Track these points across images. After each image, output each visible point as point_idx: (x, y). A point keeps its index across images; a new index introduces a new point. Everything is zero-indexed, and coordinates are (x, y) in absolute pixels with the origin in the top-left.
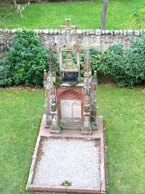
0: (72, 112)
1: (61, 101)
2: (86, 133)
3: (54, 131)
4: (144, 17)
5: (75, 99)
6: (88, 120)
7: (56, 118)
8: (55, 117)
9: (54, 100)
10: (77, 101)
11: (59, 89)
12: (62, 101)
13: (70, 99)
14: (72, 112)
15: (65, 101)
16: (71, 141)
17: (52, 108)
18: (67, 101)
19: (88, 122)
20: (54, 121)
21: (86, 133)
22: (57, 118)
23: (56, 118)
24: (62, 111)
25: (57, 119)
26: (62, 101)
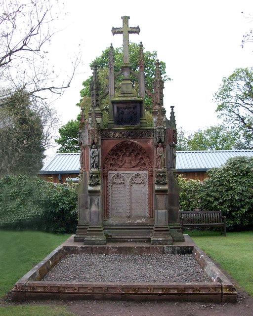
0: (131, 203)
1: (109, 172)
2: (161, 239)
3: (93, 239)
4: (125, 315)
5: (136, 168)
6: (164, 208)
7: (98, 203)
8: (96, 203)
9: (97, 159)
10: (140, 172)
11: (106, 142)
12: (112, 174)
13: (129, 168)
14: (131, 203)
15: (116, 173)
16: (133, 27)
17: (91, 177)
18: (120, 172)
19: (164, 211)
20: (95, 212)
21: (161, 239)
22: (100, 204)
23: (98, 203)
24: (110, 197)
25: (100, 207)
26: (112, 174)
